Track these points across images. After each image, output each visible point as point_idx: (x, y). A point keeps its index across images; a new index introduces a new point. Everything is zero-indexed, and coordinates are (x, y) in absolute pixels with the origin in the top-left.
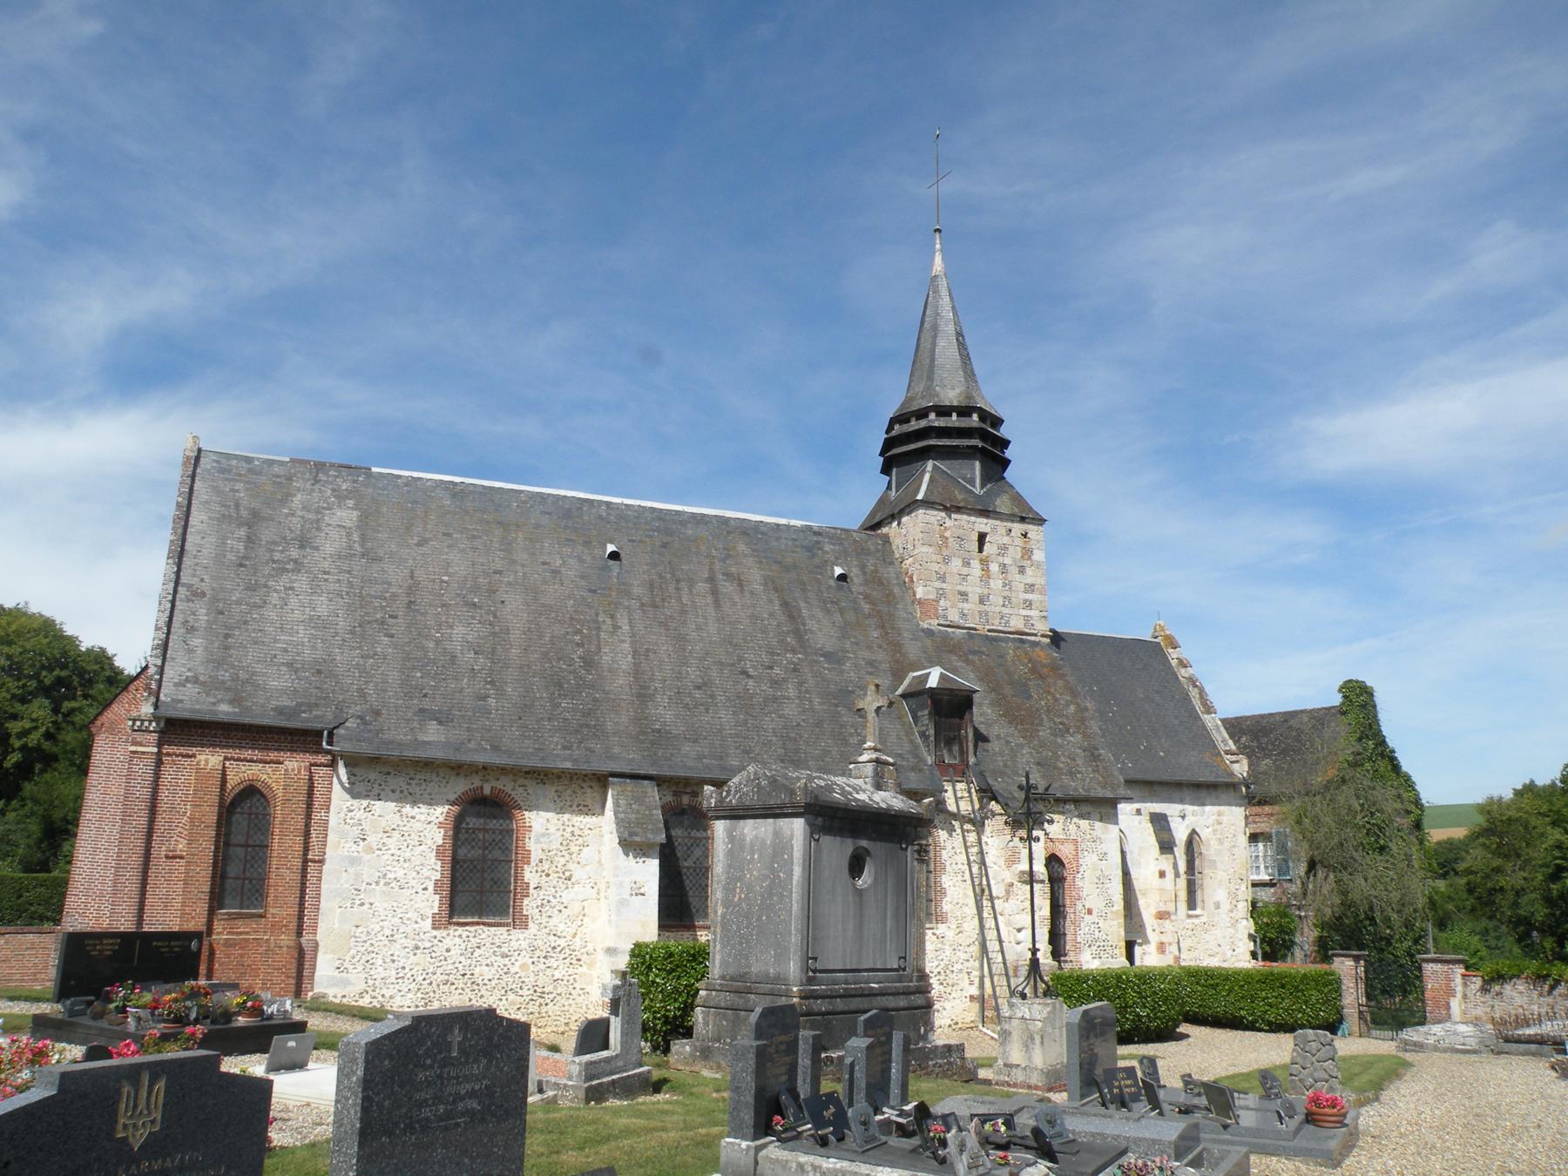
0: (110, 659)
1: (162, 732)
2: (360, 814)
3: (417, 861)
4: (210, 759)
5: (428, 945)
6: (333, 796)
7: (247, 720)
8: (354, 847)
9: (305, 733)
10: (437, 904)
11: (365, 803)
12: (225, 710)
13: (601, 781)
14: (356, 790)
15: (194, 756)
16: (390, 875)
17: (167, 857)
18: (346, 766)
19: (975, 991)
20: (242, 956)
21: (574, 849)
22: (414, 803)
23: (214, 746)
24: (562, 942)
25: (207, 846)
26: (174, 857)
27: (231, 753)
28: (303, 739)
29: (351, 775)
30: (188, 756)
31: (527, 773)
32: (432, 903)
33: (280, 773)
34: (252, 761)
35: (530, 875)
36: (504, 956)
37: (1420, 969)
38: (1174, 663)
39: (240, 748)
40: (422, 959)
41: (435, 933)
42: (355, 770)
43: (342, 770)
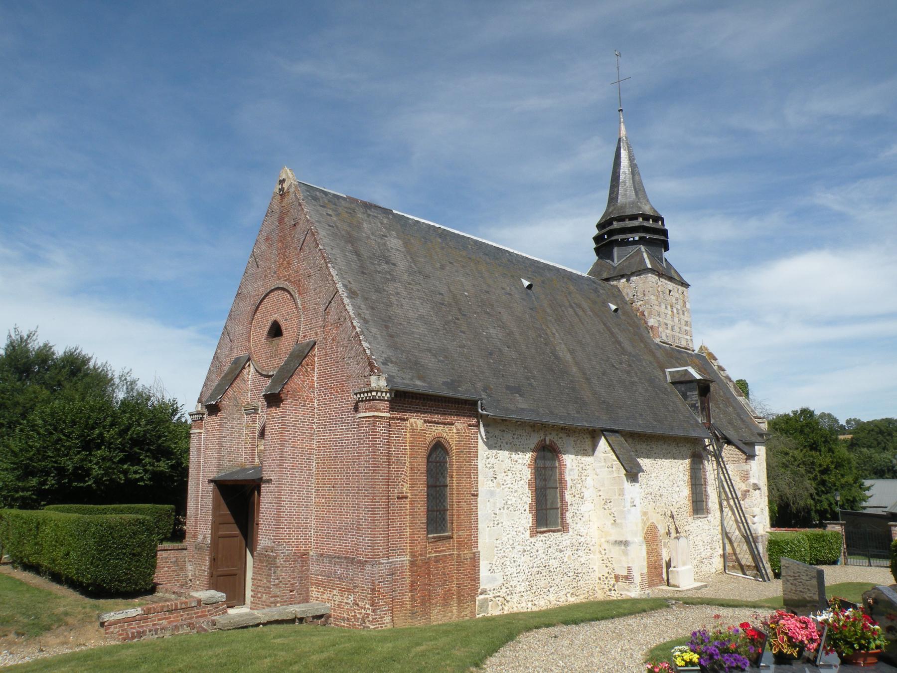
0: (85, 361)
1: (391, 401)
2: (492, 460)
3: (520, 491)
4: (416, 421)
5: (529, 548)
6: (479, 448)
7: (431, 392)
8: (492, 484)
9: (465, 402)
10: (531, 520)
11: (494, 451)
12: (450, 394)
13: (594, 435)
14: (490, 443)
15: (407, 420)
16: (509, 502)
17: (398, 498)
18: (484, 426)
19: (721, 552)
20: (444, 567)
21: (584, 478)
22: (516, 451)
23: (417, 412)
24: (582, 539)
25: (422, 488)
26: (402, 498)
27: (428, 417)
28: (465, 407)
29: (487, 432)
30: (404, 420)
31: (562, 429)
32: (527, 520)
33: (454, 430)
34: (438, 423)
35: (568, 498)
36: (561, 551)
37: (156, 555)
38: (716, 368)
39: (431, 413)
40: (527, 558)
41: (533, 540)
42: (490, 429)
43: (482, 429)
